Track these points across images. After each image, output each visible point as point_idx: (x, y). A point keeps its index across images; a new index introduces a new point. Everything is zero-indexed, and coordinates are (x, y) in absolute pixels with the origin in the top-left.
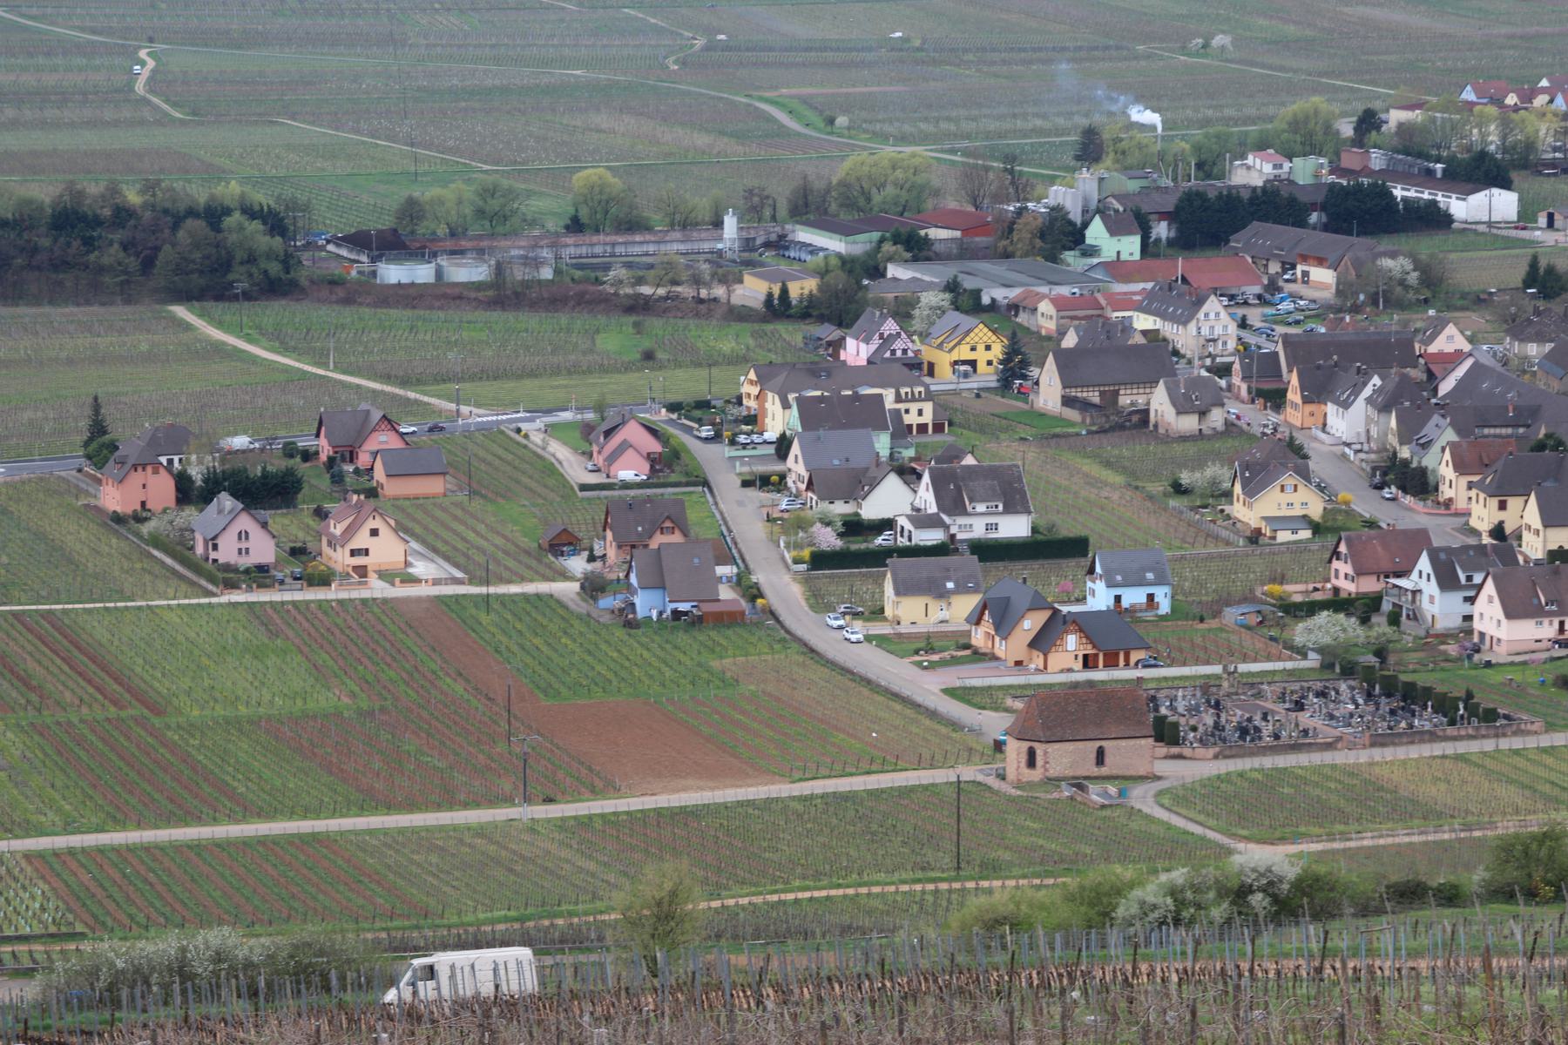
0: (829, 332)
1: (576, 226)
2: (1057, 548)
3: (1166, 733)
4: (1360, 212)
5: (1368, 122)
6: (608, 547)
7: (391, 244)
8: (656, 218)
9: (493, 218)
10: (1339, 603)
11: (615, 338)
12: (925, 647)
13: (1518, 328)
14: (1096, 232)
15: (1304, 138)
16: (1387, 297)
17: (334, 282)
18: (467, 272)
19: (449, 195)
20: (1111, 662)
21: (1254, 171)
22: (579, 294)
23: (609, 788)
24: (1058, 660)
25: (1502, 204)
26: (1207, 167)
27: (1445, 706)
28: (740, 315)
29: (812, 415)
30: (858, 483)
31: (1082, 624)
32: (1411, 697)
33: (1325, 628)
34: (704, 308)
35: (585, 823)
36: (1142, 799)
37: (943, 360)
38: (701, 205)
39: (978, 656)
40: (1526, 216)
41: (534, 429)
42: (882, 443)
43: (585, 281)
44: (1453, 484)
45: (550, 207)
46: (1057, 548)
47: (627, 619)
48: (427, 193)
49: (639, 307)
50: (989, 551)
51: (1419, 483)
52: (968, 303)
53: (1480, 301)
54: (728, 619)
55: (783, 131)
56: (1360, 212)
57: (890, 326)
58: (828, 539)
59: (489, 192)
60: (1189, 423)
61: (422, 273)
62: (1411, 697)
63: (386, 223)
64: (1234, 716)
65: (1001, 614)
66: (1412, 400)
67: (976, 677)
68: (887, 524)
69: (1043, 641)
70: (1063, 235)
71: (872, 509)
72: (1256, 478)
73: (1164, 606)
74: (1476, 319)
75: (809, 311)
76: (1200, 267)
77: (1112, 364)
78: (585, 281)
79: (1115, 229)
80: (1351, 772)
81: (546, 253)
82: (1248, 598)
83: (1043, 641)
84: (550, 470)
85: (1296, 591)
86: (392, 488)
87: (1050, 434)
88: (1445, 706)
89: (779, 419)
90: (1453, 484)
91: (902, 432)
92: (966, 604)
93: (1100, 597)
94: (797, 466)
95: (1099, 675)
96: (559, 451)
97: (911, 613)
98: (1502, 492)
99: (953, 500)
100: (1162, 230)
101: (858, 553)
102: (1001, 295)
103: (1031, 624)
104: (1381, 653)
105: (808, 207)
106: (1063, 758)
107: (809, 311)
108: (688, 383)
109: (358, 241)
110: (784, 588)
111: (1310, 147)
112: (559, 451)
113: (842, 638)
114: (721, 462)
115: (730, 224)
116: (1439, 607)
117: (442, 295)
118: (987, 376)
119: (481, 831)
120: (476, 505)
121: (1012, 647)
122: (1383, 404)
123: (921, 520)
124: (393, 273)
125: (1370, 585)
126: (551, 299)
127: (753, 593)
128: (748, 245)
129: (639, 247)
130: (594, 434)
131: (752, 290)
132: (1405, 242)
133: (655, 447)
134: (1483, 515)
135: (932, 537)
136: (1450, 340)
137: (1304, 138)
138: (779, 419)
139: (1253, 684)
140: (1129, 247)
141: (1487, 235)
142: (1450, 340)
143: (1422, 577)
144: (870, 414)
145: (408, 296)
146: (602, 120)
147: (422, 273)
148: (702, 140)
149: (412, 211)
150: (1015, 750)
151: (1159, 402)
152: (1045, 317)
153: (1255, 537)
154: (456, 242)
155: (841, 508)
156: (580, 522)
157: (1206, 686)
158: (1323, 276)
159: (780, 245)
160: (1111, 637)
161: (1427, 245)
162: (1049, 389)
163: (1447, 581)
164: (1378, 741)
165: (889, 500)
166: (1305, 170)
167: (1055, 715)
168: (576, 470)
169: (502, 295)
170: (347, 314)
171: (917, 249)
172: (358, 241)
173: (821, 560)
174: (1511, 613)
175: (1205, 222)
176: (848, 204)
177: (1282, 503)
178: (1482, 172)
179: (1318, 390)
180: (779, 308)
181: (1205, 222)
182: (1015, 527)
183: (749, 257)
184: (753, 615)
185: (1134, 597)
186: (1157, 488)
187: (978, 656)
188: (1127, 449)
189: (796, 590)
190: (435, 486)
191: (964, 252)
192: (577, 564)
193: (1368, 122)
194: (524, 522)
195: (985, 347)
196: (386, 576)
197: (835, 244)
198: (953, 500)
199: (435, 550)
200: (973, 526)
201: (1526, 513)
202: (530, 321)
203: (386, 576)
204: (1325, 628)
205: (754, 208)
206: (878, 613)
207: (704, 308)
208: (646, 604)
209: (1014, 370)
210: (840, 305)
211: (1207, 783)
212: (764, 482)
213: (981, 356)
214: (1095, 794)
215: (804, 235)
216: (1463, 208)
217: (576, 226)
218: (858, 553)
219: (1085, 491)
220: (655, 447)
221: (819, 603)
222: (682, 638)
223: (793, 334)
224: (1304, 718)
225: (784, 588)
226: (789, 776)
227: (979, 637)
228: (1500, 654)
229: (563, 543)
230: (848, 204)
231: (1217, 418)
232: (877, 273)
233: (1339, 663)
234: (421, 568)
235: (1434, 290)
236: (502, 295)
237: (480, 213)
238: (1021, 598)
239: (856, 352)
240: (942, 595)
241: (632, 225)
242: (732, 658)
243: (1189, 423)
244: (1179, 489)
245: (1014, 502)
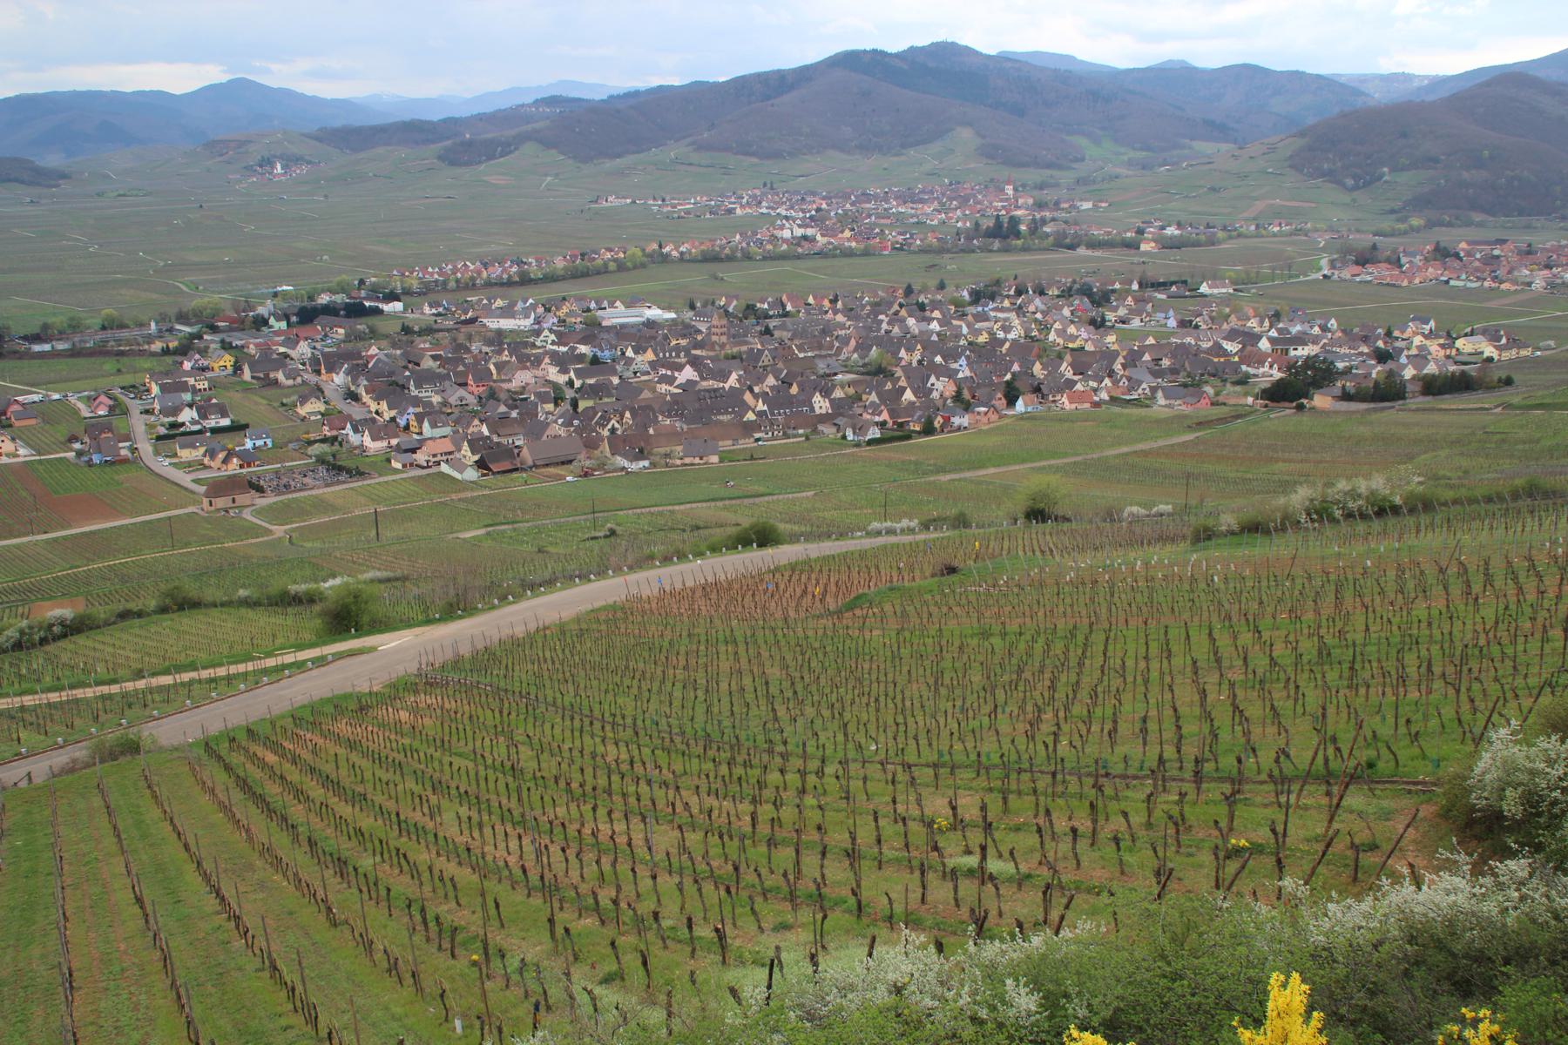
0: (179, 359)
1: (104, 328)
2: (238, 428)
3: (260, 489)
4: (355, 311)
5: (362, 282)
6: (87, 439)
7: (37, 338)
8: (130, 323)
9: (75, 326)
10: (324, 440)
11: (110, 365)
12: (188, 466)
13: (394, 346)
14: (272, 321)
15: (342, 289)
16: (360, 337)
17: (15, 352)
18: (61, 346)
19: (58, 320)
20: (249, 465)
21: (324, 299)
22: (100, 352)
23: (70, 526)
24: (231, 467)
25: (398, 306)
26: (311, 298)
27: (349, 471)
28: (153, 354)
29: (163, 388)
30: (176, 411)
31: (239, 455)
32: (340, 469)
33: (317, 449)
34: (142, 353)
35: (55, 540)
36: (247, 515)
37: (216, 366)
38: (144, 318)
39: (206, 467)
40: (405, 309)
41: (73, 399)
42: (187, 397)
43: (105, 347)
44: (366, 398)
45: (96, 322)
46: (238, 428)
47: (90, 464)
48: (51, 320)
49: (121, 354)
50: (216, 431)
51: (355, 397)
52: (226, 346)
53: (387, 336)
54: (125, 461)
55: (182, 292)
56: (355, 311)
57: (197, 356)
58: (163, 431)
59: (72, 319)
60: (290, 382)
61: (47, 347)
62: (340, 469)
63: (36, 330)
64: (284, 480)
65: (212, 453)
66: (354, 373)
67: (203, 475)
68: (183, 424)
69: (225, 461)
70: (261, 322)
71: (180, 419)
72: (304, 400)
73: (270, 445)
74: (384, 343)
75: (176, 352)
76: (305, 330)
77: (269, 361)
78: (105, 347)
79: (278, 320)
80: (316, 497)
81: (1009, 190)
82: (298, 440)
83: (225, 461)
84: (76, 412)
85: (312, 436)
86: (17, 424)
87: (247, 389)
88: (349, 471)
89: (155, 389)
90: (366, 398)
91: (195, 391)
92: (202, 450)
93: (249, 444)
94: (157, 407)
95: (244, 471)
96: (80, 405)
97: (186, 454)
98: (378, 399)
99: (203, 414)
100: (294, 319)
101: (175, 433)
102: (239, 343)
103: (221, 456)
104: (334, 456)
105: (183, 318)
106: (221, 502)
107: (176, 352)
108: (128, 379)
109: (25, 338)
110: (146, 448)
111: (343, 291)
112: (80, 405)
113: (163, 465)
114: (135, 406)
115: (153, 325)
116: (354, 439)
117: (54, 354)
118: (230, 369)
119: (18, 547)
120: (47, 427)
121: (216, 464)
122: (347, 373)
123: (194, 422)
124: (37, 348)
125: (335, 433)
126: (91, 353)
127: (134, 450)
128: (160, 331)
129: (125, 334)
130: (90, 400)
131: (157, 346)
132: (364, 320)
133: (111, 403)
134: (373, 407)
135: (196, 428)
136: (373, 350)
137: (342, 289)
138: (155, 389)
139: (291, 470)
140: (283, 325)
141: (394, 316)
142: (373, 350)
143: (348, 429)
144: (184, 387)
145: (42, 355)
146: (123, 292)
147: (47, 347)
148: (155, 296)
149: (45, 327)
150: (206, 501)
151: (280, 376)
152: (252, 350)
153: (303, 419)
154: (62, 335)
155: (171, 419)
156: (80, 431)
157: (277, 472)
158: (341, 331)
159: (171, 330)
160: (247, 459)
161: (374, 321)
162: (247, 375)
163: (356, 430)
164: (327, 485)
165: (187, 415)
166: (340, 298)
167: (219, 488)
168: (85, 413)
169: (74, 353)
170: (18, 363)
171: (214, 329)
172: (25, 338)
173: (159, 438)
174: (373, 439)
175: (308, 315)
176: (195, 315)
177: (313, 407)
178: (392, 297)
179: (330, 370)
180: (166, 352)
181: (308, 315)
182: (226, 422)
183: (160, 335)
184: (134, 461)
185: (259, 443)
186: (276, 404)
187: (206, 467)
188: (272, 392)
189: (150, 449)
190: (33, 422)
191: (230, 329)
192: (77, 446)
193: (362, 282)
194: (62, 432)
195: (228, 360)
196: (8, 455)
197: (188, 329)
198: (203, 414)
199: (28, 445)
200: (213, 422)
201: (384, 406)
202: (81, 361)
203: (8, 455)
204: (317, 449)
205: (162, 318)
206: (175, 455)
207: (142, 353)
208: (96, 459)
209: (237, 368)
210: (184, 350)
211: (270, 506)
212: (147, 412)
213: (228, 364)
214: (232, 513)
215: (178, 327)
216: (388, 308)
217: (104, 328)
218: (175, 433)
219: (255, 407)
220: (111, 403)
221: (157, 453)
222: (108, 469)
223: (169, 359)
224: (306, 480)
225: (146, 448)
226: (132, 515)
227: (206, 461)
228: (371, 452)
229: (73, 438)
230: (195, 315)
231: (299, 380)
232: (200, 337)
233: (321, 460)
234: (22, 451)
235: (374, 334)
236: (74, 353)
237: (70, 326)
238: (218, 447)
239: (187, 365)
240: (195, 448)
241: (122, 326)
242: (122, 474)
243: (290, 382)
244: (283, 405)
245: (224, 414)
